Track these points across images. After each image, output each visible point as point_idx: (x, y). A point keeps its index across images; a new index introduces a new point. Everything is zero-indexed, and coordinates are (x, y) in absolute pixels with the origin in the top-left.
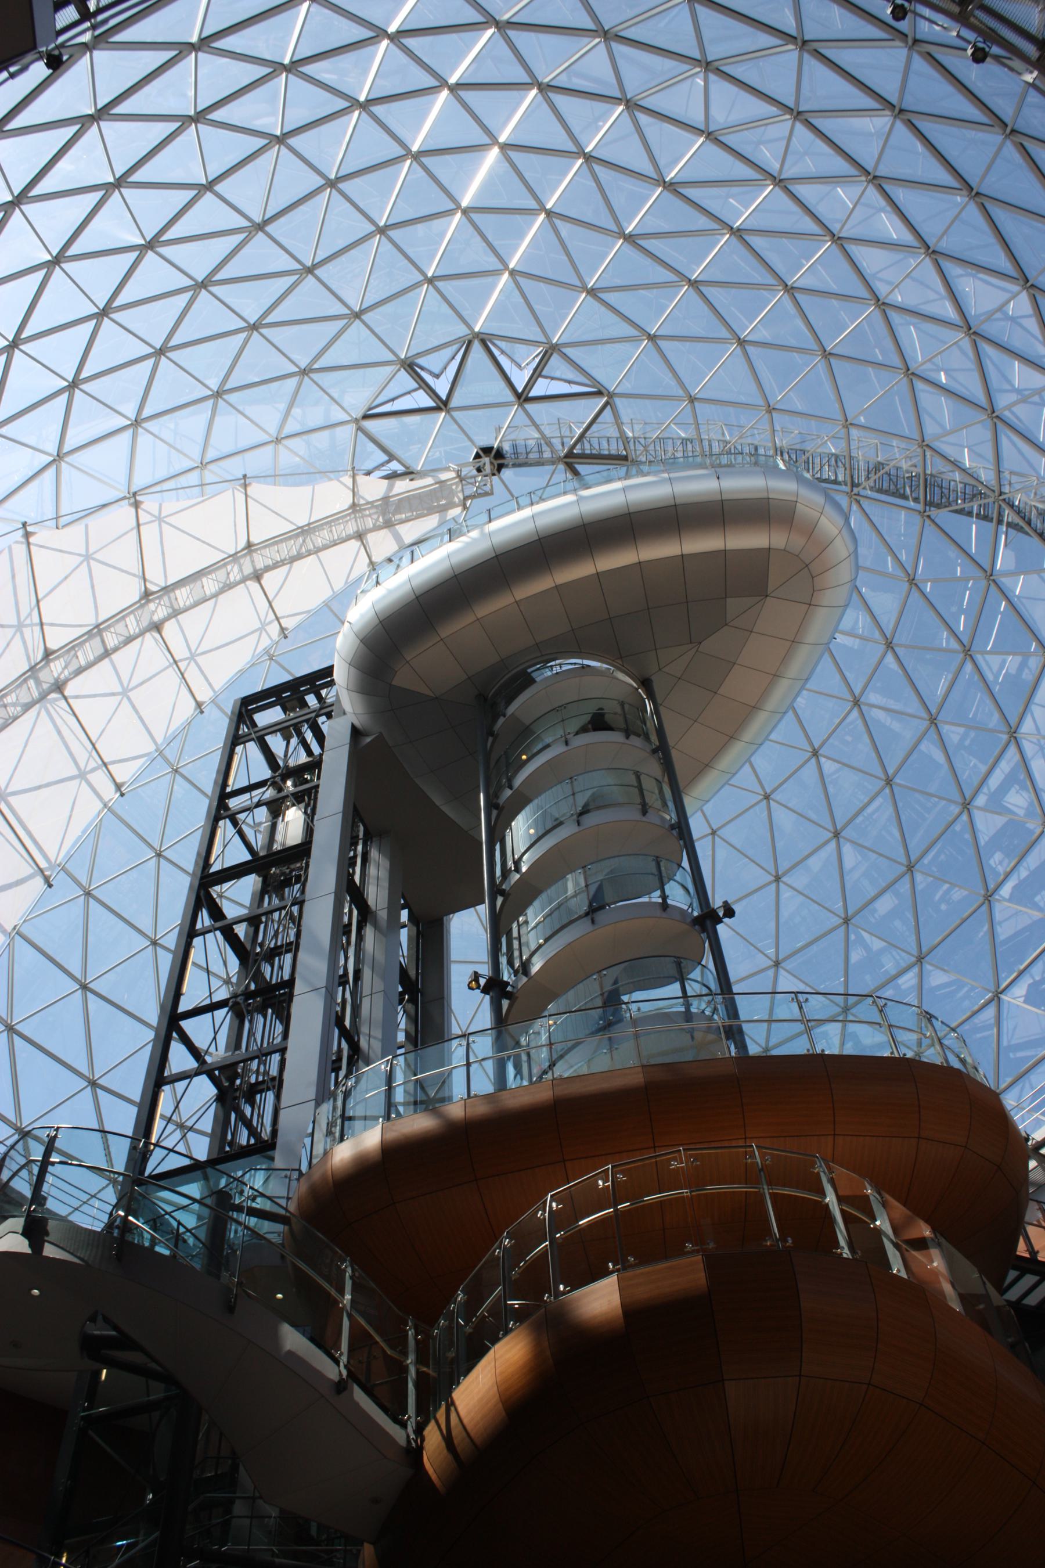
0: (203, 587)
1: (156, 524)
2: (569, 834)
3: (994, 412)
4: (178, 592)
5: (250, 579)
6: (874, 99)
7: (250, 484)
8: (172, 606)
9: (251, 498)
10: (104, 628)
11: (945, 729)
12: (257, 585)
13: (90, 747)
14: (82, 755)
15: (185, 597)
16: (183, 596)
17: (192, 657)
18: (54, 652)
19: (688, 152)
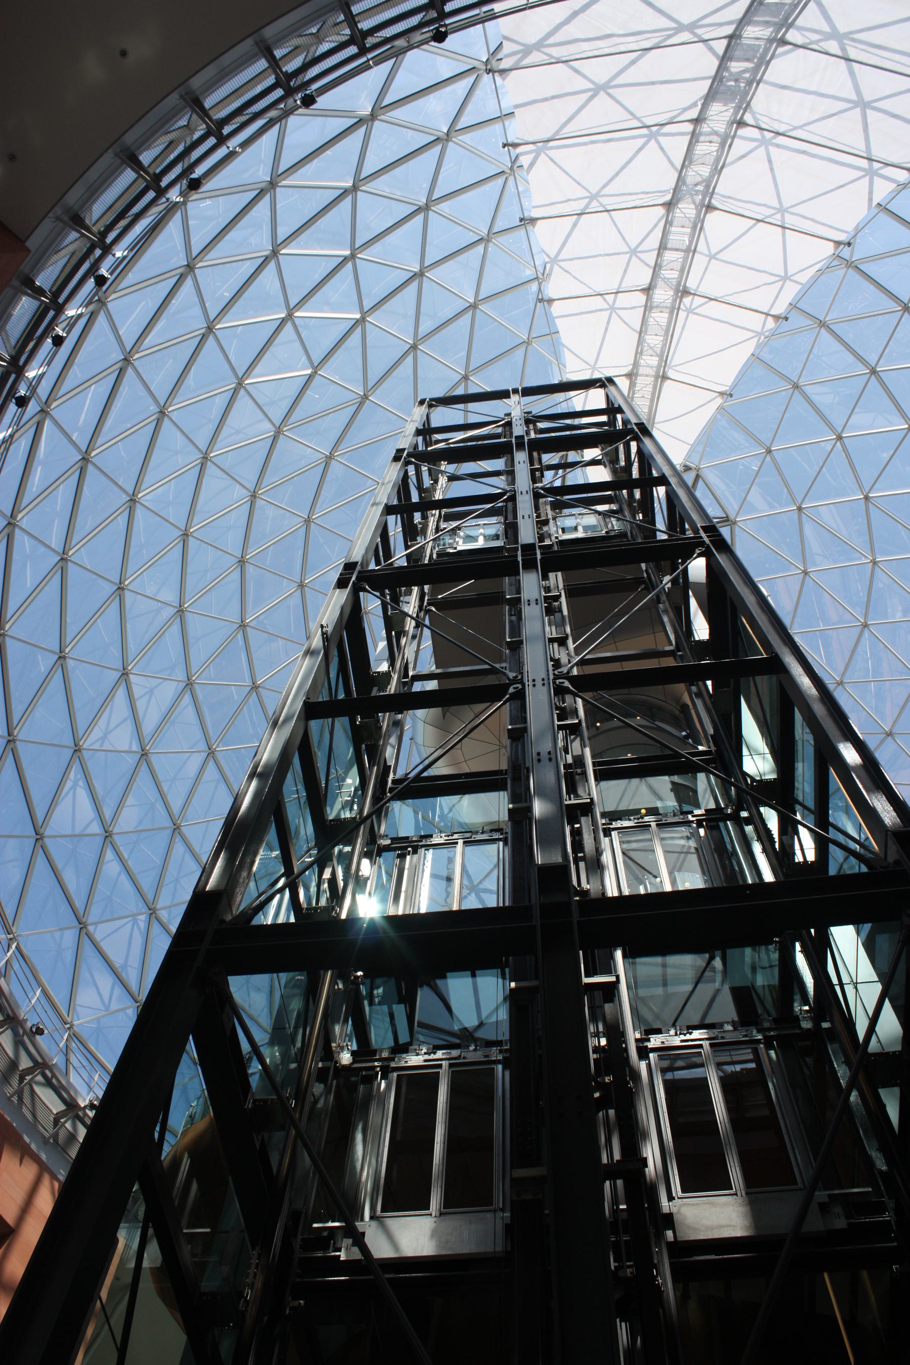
0: (656, 335)
1: (786, 205)
2: (664, 1186)
3: (81, 928)
4: (666, 315)
5: (632, 370)
6: (468, 76)
7: (723, 398)
8: (657, 307)
9: (754, 225)
10: (657, 381)
11: (170, 595)
12: (624, 373)
13: (609, 208)
14: (598, 302)
15: (657, 319)
16: (659, 318)
17: (612, 309)
18: (662, 382)
19: (829, 1293)
